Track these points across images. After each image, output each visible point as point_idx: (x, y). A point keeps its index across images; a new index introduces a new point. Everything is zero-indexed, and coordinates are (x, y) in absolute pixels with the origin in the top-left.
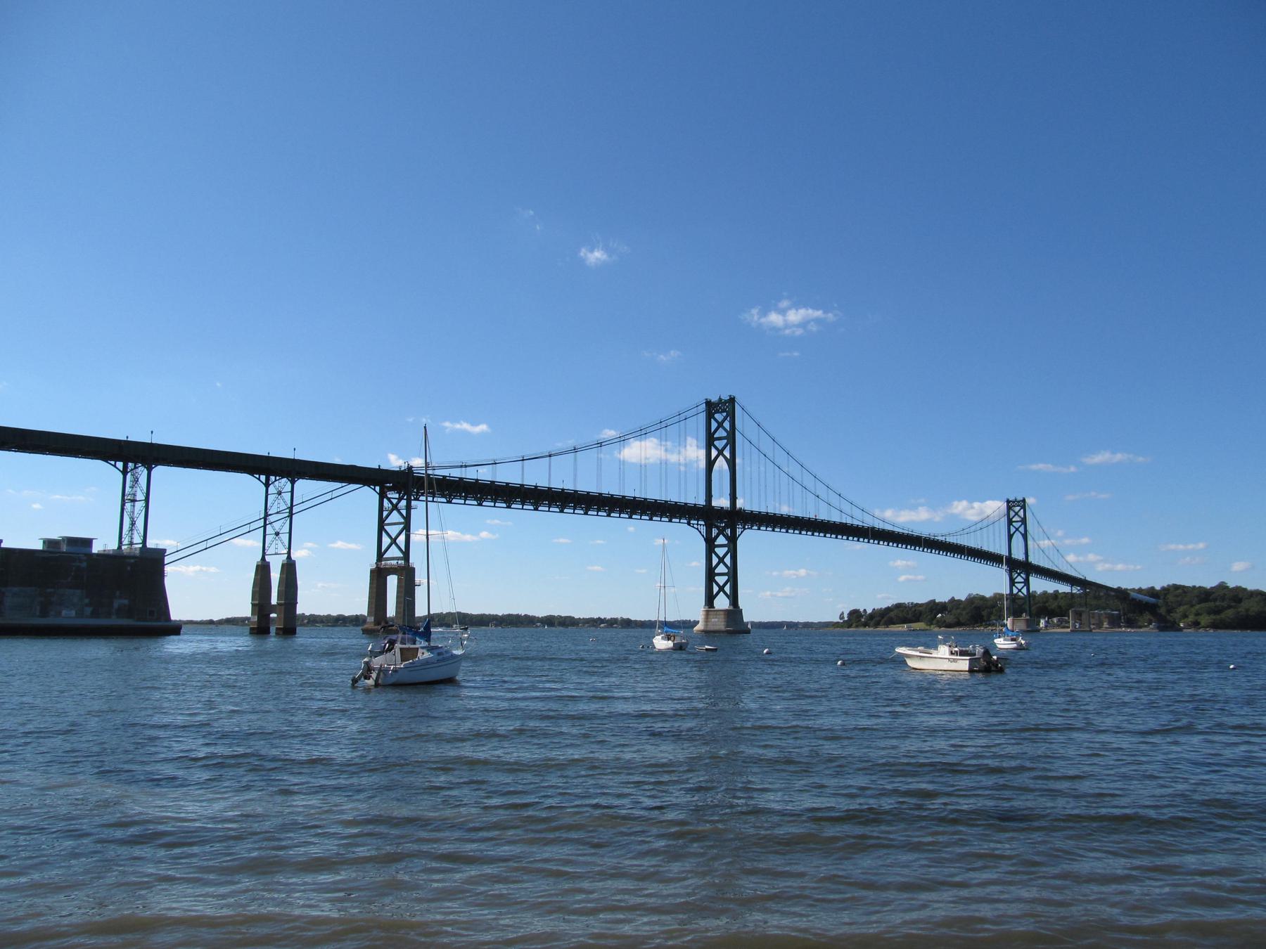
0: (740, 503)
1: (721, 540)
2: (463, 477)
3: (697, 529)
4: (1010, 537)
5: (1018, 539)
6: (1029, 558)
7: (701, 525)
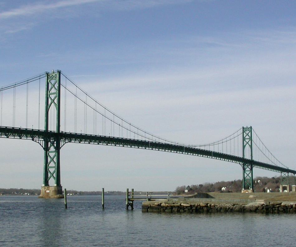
0: (62, 129)
3: (39, 143)
4: (244, 147)
5: (247, 147)
6: (253, 158)
7: (41, 140)
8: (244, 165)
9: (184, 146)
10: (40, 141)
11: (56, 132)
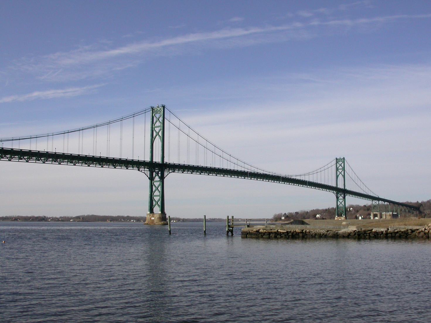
0: (166, 160)
1: (157, 178)
2: (94, 155)
3: (144, 173)
4: (337, 177)
5: (340, 177)
7: (146, 171)
8: (337, 194)
9: (281, 176)
10: (145, 171)
11: (160, 163)
